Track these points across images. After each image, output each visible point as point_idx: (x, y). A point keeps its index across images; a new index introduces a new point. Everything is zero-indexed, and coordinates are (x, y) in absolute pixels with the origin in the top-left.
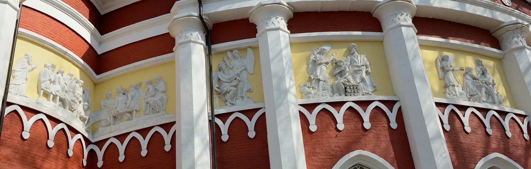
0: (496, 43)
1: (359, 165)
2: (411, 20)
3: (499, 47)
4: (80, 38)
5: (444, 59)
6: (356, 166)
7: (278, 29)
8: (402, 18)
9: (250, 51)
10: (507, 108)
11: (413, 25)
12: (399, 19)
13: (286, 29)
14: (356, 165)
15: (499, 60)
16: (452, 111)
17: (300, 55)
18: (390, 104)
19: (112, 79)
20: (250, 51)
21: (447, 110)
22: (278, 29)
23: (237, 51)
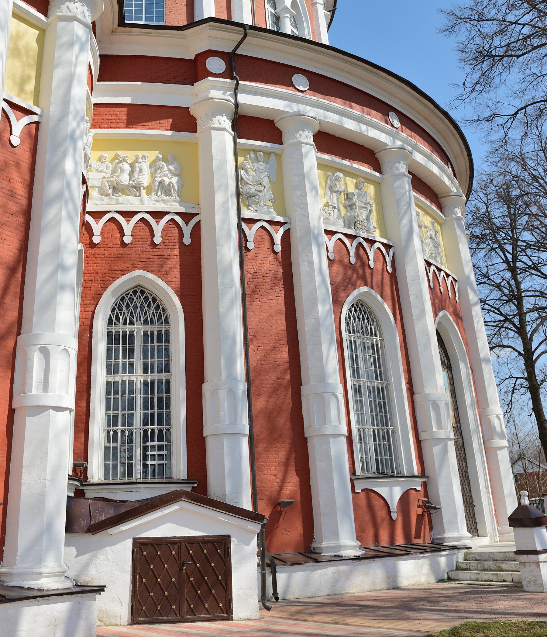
0: (377, 166)
1: (140, 286)
2: (312, 137)
3: (380, 172)
4: (249, 319)
5: (490, 168)
6: (136, 289)
7: (224, 129)
8: (304, 135)
9: (273, 157)
10: (377, 235)
11: (313, 143)
12: (300, 135)
13: (230, 130)
14: (137, 287)
15: (378, 184)
16: (360, 244)
17: (321, 172)
18: (388, 247)
19: (332, 67)
20: (273, 157)
21: (355, 243)
22: (224, 129)
23: (261, 153)
